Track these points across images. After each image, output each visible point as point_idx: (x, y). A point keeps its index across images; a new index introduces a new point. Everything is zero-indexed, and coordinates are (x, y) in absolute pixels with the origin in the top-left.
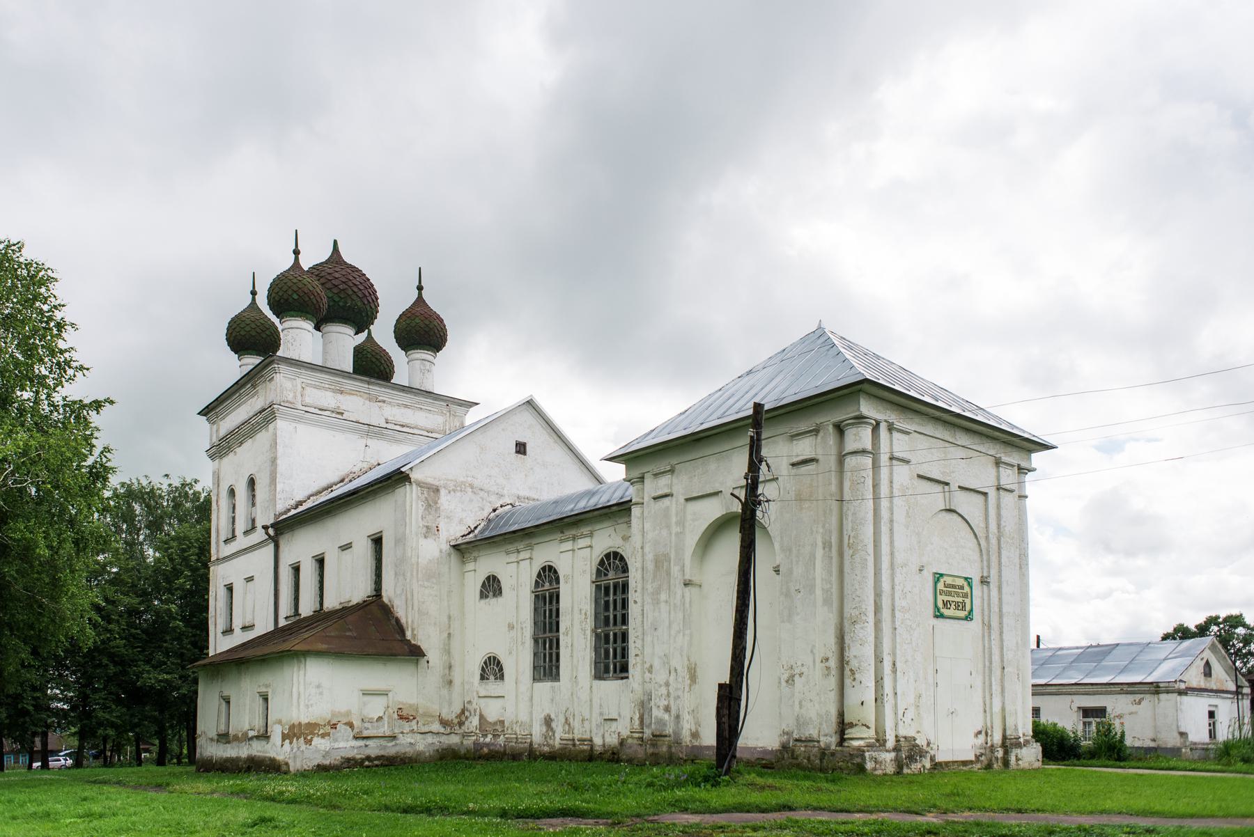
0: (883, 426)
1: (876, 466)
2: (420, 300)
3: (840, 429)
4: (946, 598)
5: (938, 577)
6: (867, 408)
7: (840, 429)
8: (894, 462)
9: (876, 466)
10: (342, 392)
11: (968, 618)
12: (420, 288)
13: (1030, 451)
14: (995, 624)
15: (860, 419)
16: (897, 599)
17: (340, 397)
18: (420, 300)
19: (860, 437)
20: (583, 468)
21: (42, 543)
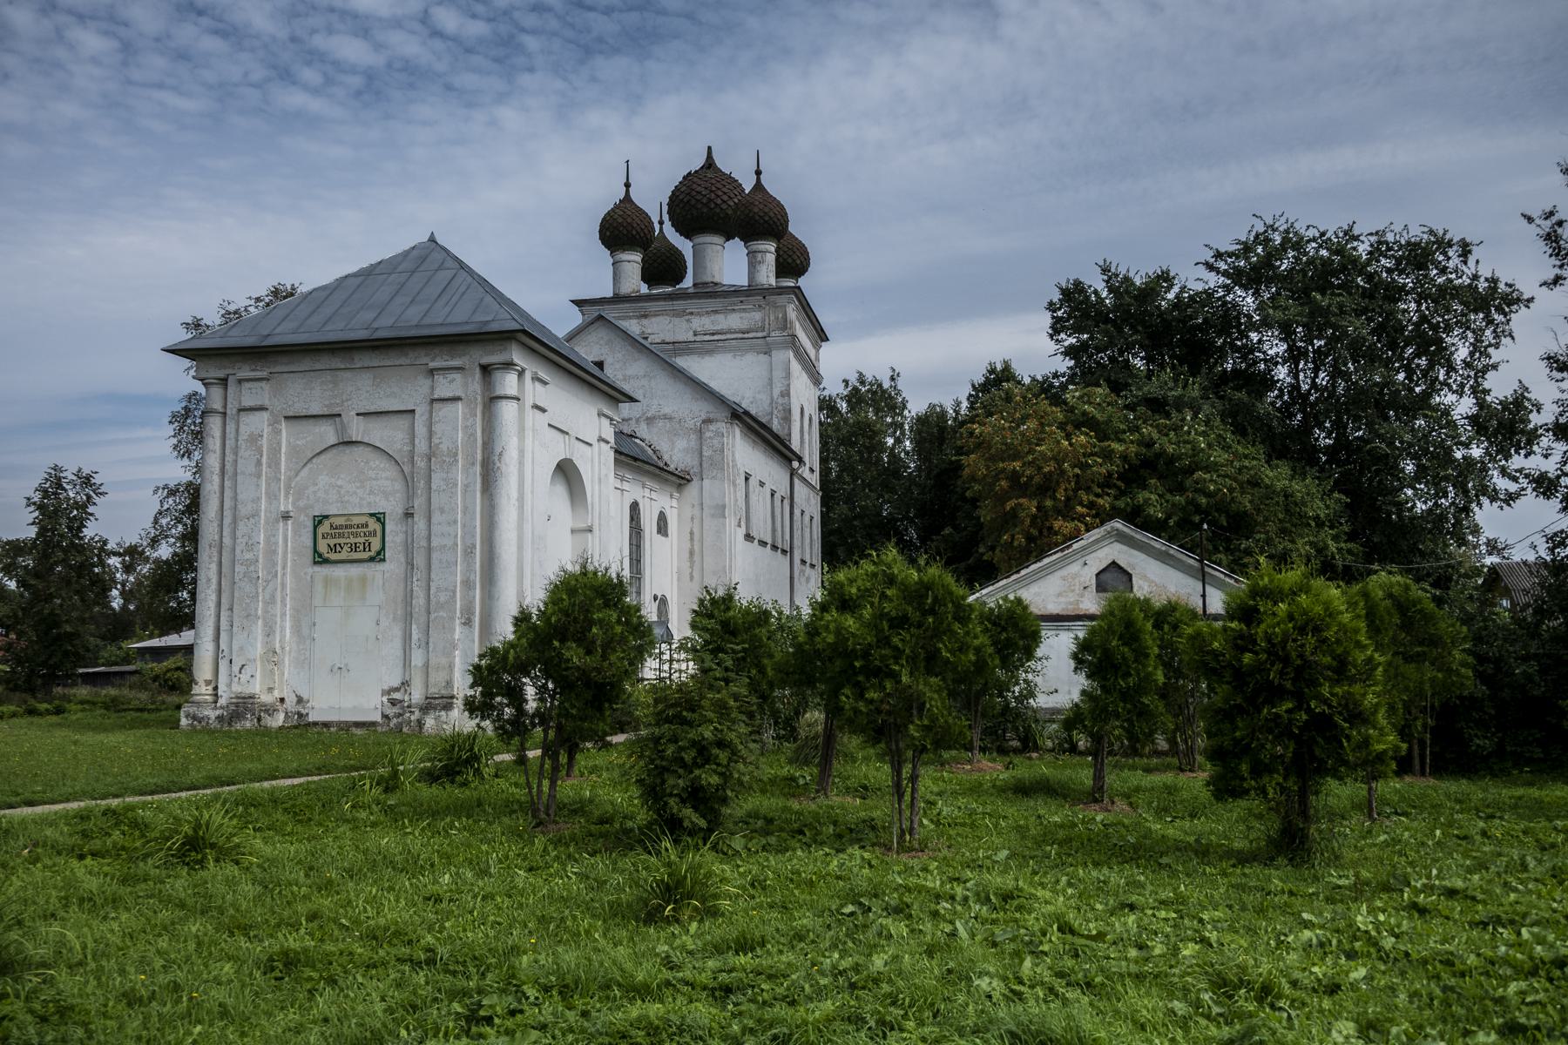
0: (528, 375)
1: (521, 411)
2: (627, 197)
3: (486, 370)
4: (332, 542)
5: (319, 520)
6: (518, 357)
7: (486, 370)
8: (436, 406)
9: (521, 411)
10: (645, 316)
11: (379, 557)
12: (627, 185)
13: (619, 401)
14: (420, 560)
15: (509, 365)
16: (238, 551)
17: (645, 322)
18: (627, 197)
19: (508, 383)
20: (385, 418)
21: (927, 689)
